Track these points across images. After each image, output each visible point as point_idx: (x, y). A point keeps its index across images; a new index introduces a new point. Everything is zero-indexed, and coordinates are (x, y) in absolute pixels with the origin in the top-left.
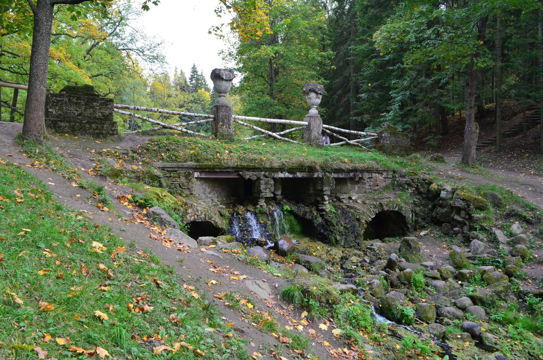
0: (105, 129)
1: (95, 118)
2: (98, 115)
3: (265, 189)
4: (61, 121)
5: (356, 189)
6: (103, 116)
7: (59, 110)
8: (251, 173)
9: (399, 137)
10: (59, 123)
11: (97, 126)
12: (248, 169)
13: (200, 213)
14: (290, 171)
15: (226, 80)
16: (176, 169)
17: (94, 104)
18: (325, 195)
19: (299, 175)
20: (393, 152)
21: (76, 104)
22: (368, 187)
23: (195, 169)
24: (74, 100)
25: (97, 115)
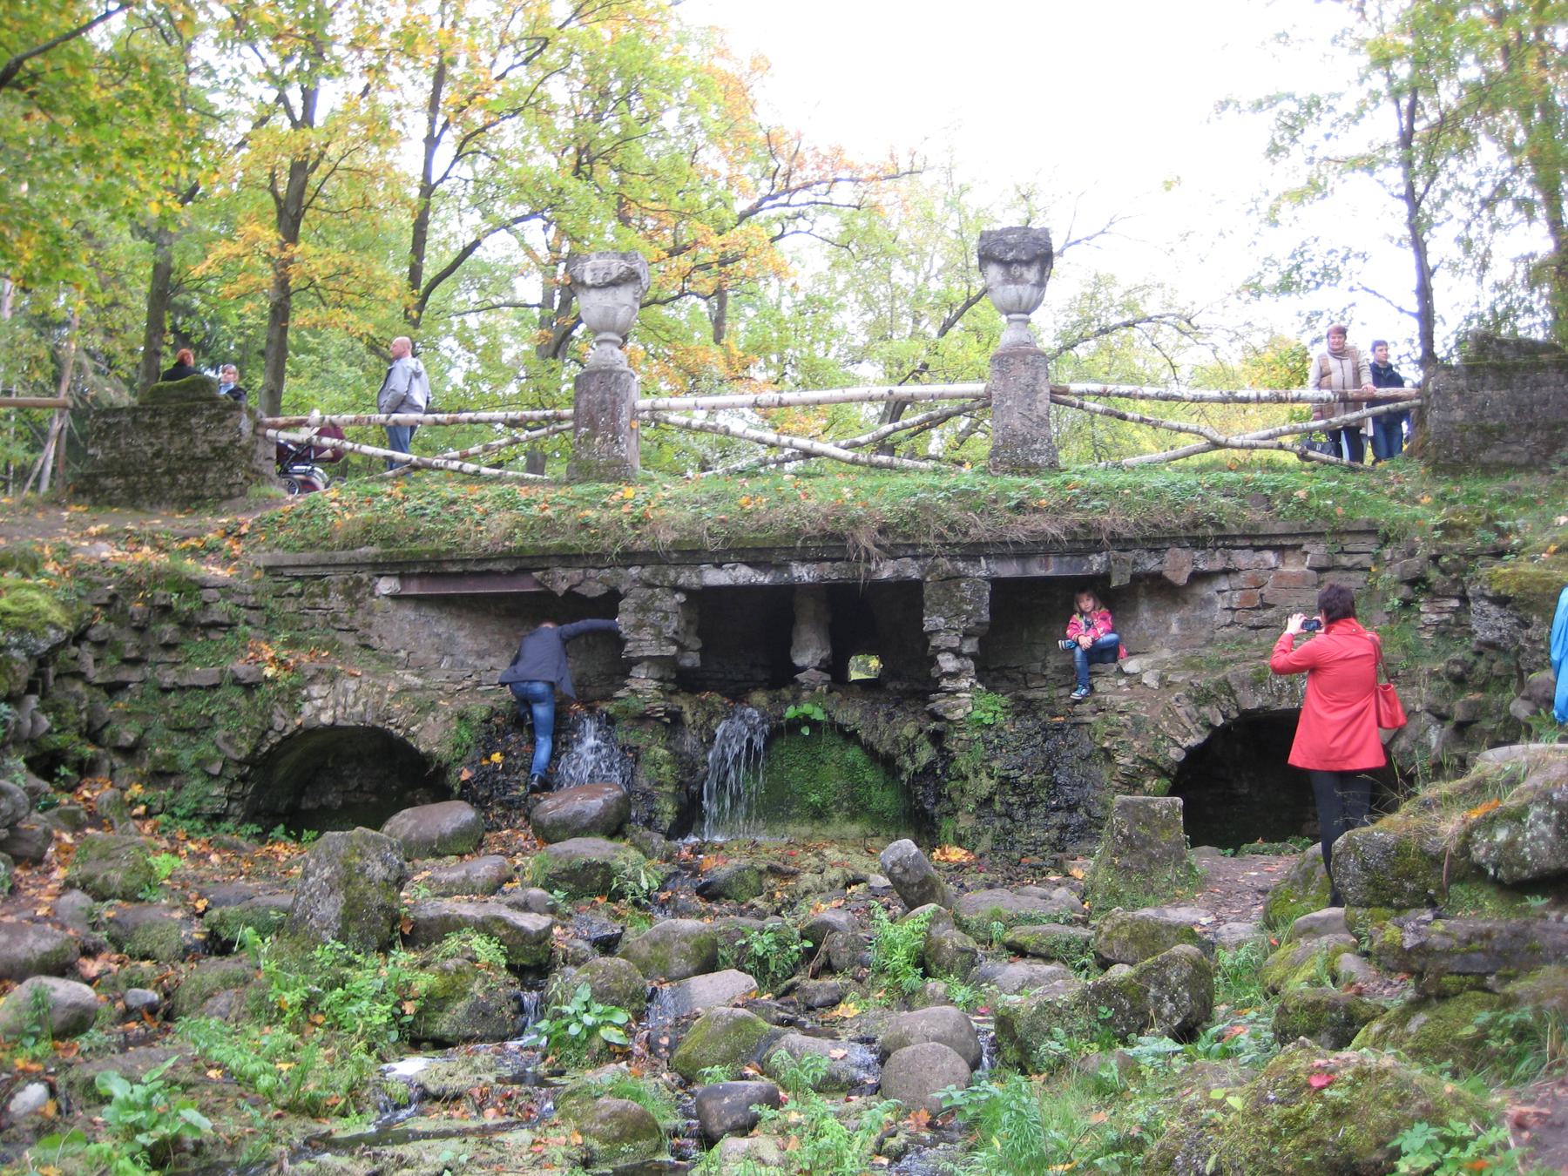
0: (210, 483)
1: (193, 458)
2: (202, 448)
3: (639, 626)
4: (107, 475)
5: (1175, 629)
6: (214, 449)
7: (112, 448)
8: (575, 574)
9: (1538, 385)
10: (102, 480)
11: (190, 479)
12: (568, 558)
13: (351, 699)
14: (756, 557)
15: (593, 286)
16: (318, 571)
17: (193, 421)
18: (938, 650)
19: (803, 573)
20: (1485, 457)
21: (150, 427)
22: (1221, 617)
23: (381, 568)
24: (146, 419)
25: (198, 451)
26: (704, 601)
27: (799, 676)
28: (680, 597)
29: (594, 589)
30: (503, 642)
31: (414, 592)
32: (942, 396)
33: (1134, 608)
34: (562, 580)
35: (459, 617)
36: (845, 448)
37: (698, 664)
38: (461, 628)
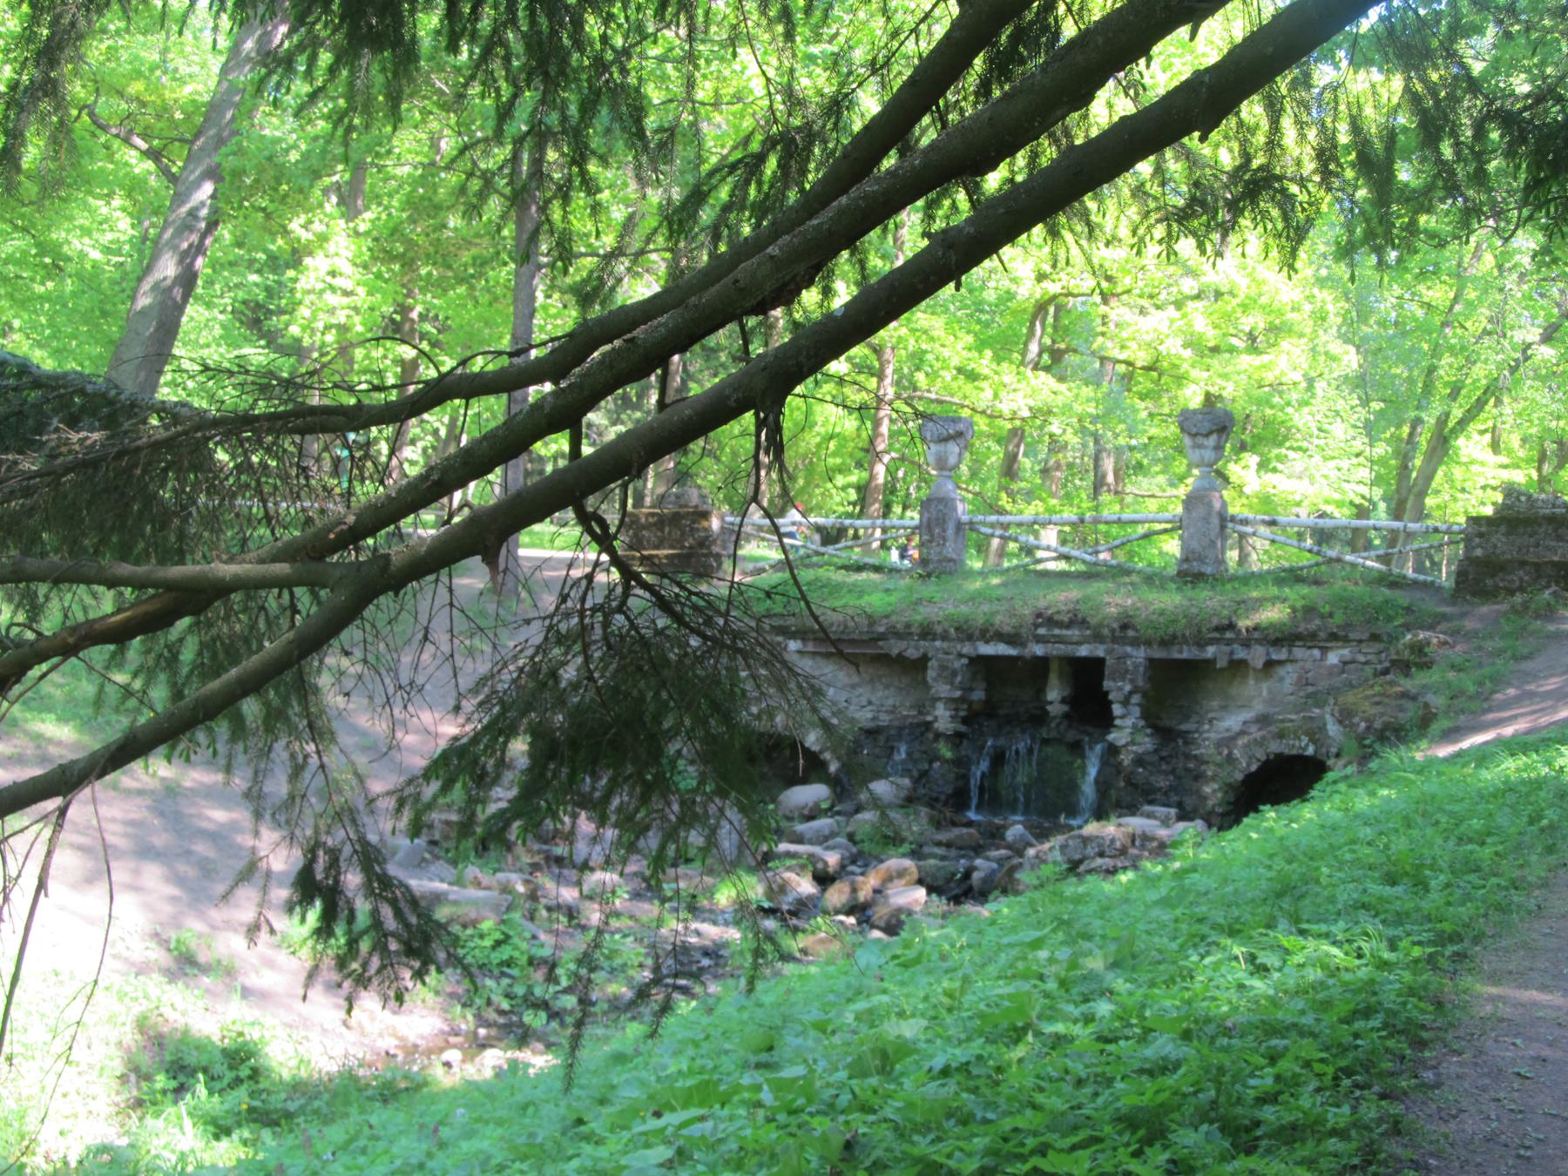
14: (1012, 639)
26: (981, 664)
28: (965, 661)
29: (912, 653)
33: (1245, 676)
34: (895, 647)
38: (841, 669)
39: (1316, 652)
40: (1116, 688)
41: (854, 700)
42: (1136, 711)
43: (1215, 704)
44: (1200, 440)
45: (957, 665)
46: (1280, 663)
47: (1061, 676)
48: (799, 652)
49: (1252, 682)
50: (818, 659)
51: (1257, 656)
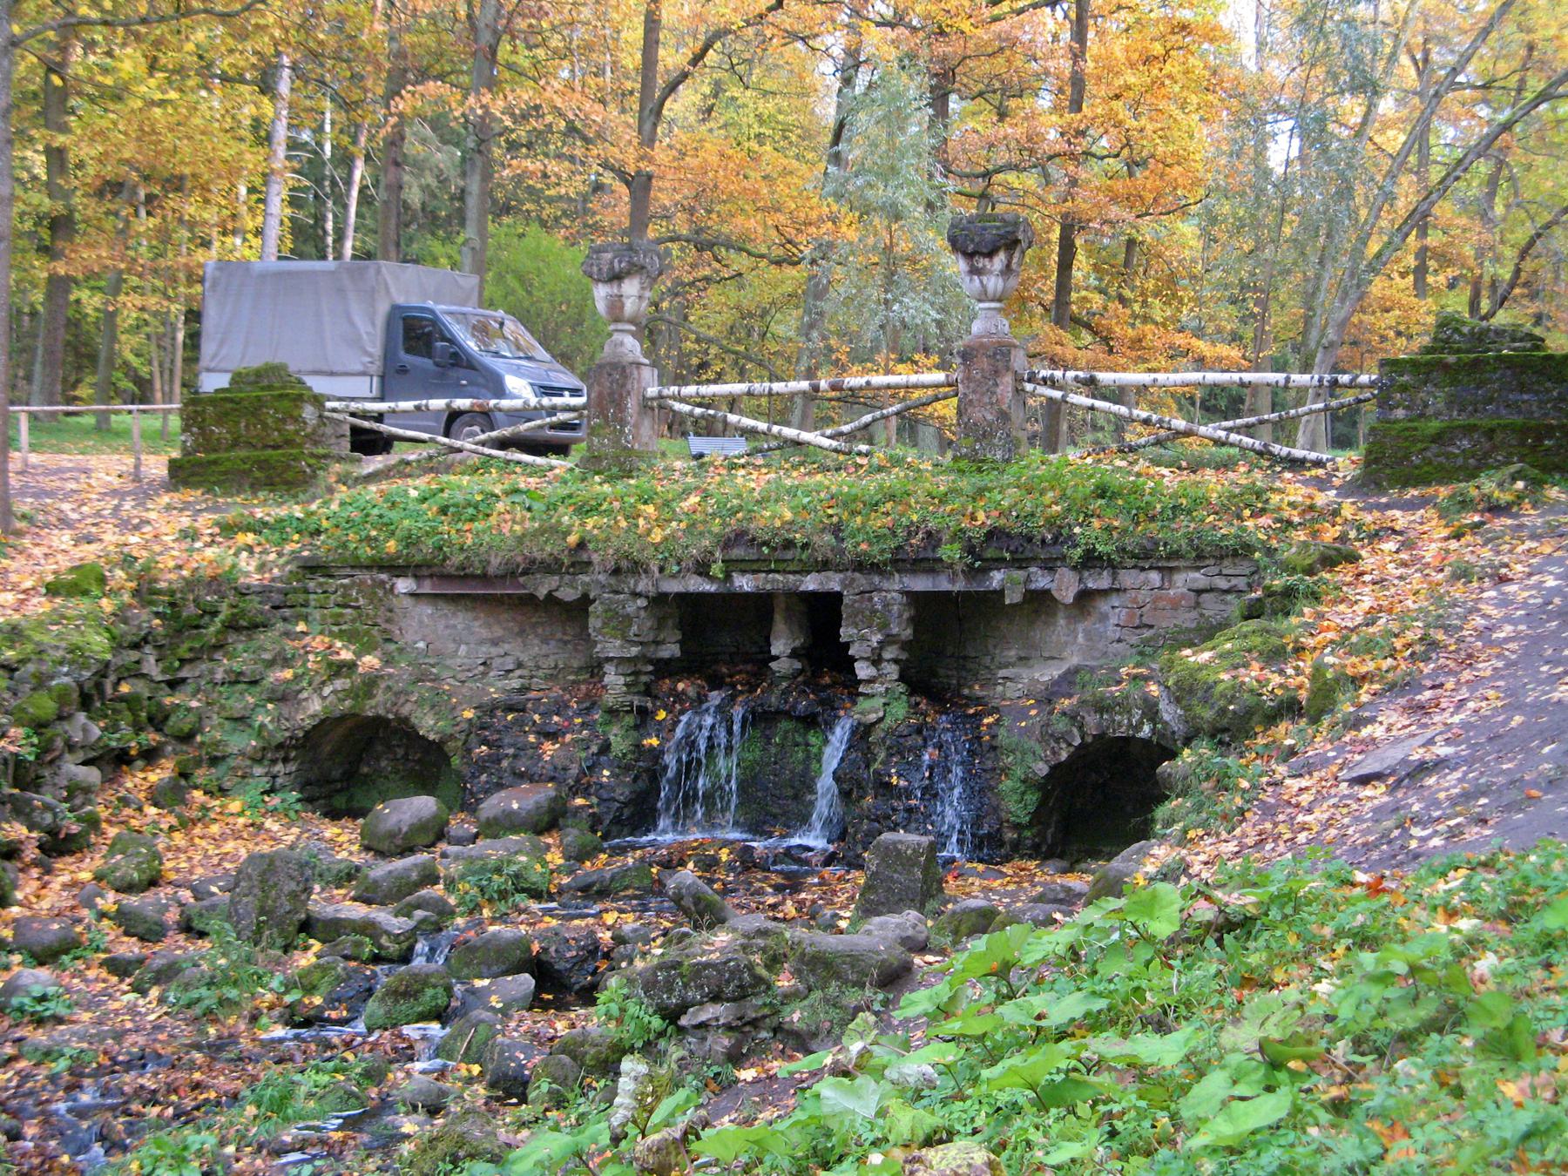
8: (554, 581)
23: (395, 568)
27: (773, 665)
29: (568, 594)
30: (516, 629)
31: (427, 590)
32: (916, 386)
33: (1055, 614)
34: (543, 586)
35: (474, 609)
36: (831, 437)
37: (678, 653)
38: (476, 619)
39: (1155, 577)
40: (859, 638)
41: (496, 662)
42: (892, 671)
43: (1012, 654)
44: (981, 262)
45: (630, 609)
46: (1104, 593)
47: (788, 619)
48: (413, 595)
49: (1062, 622)
50: (441, 604)
51: (1065, 586)
